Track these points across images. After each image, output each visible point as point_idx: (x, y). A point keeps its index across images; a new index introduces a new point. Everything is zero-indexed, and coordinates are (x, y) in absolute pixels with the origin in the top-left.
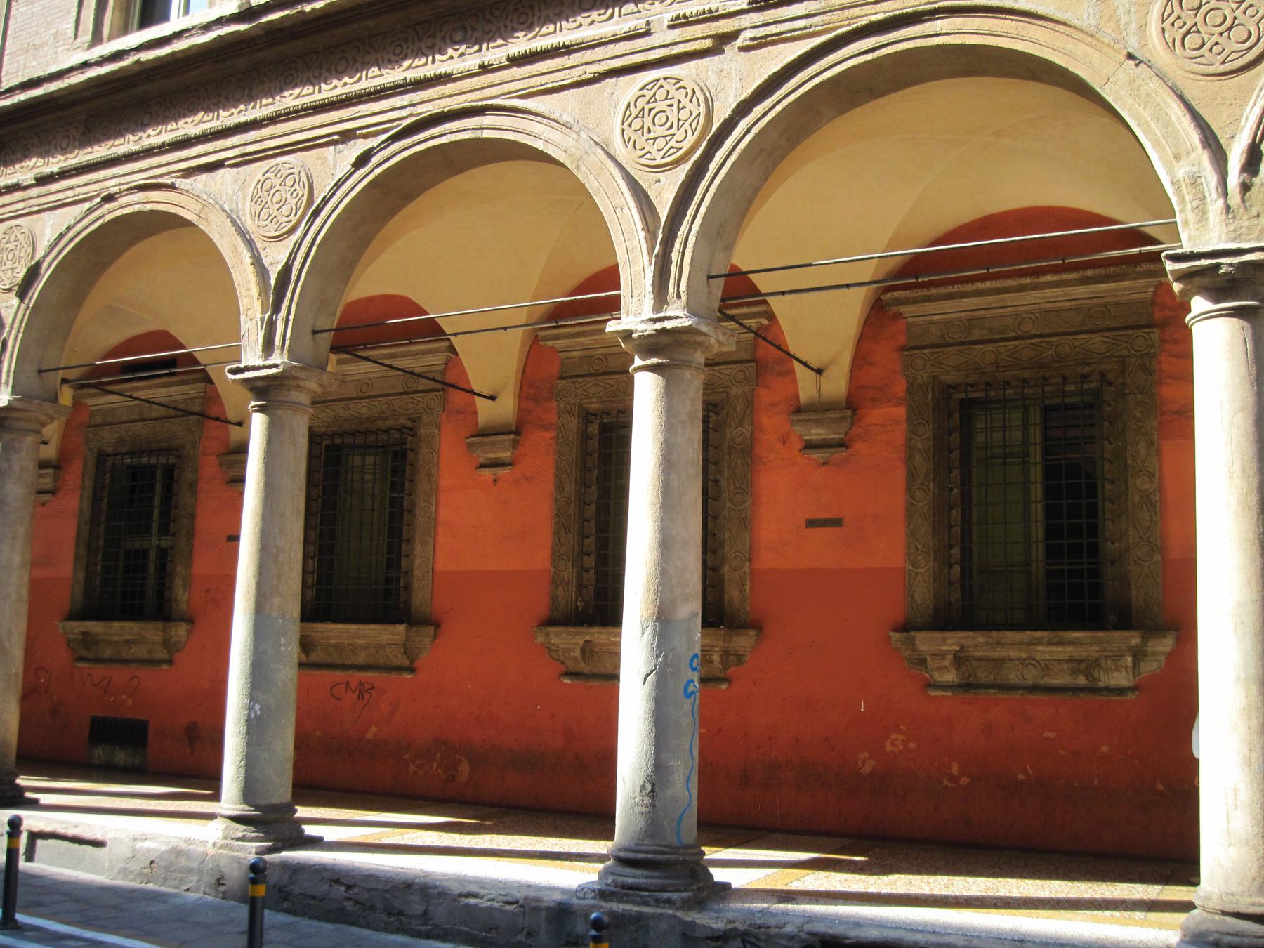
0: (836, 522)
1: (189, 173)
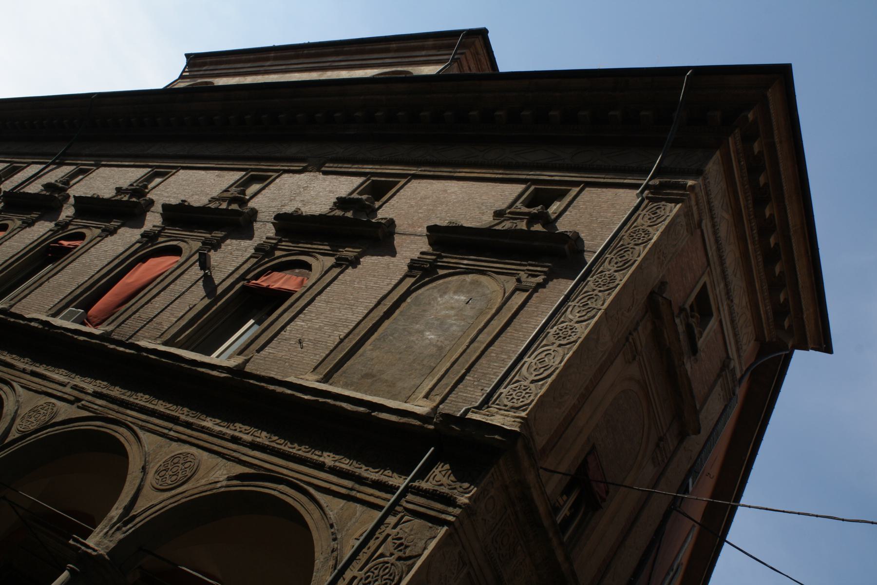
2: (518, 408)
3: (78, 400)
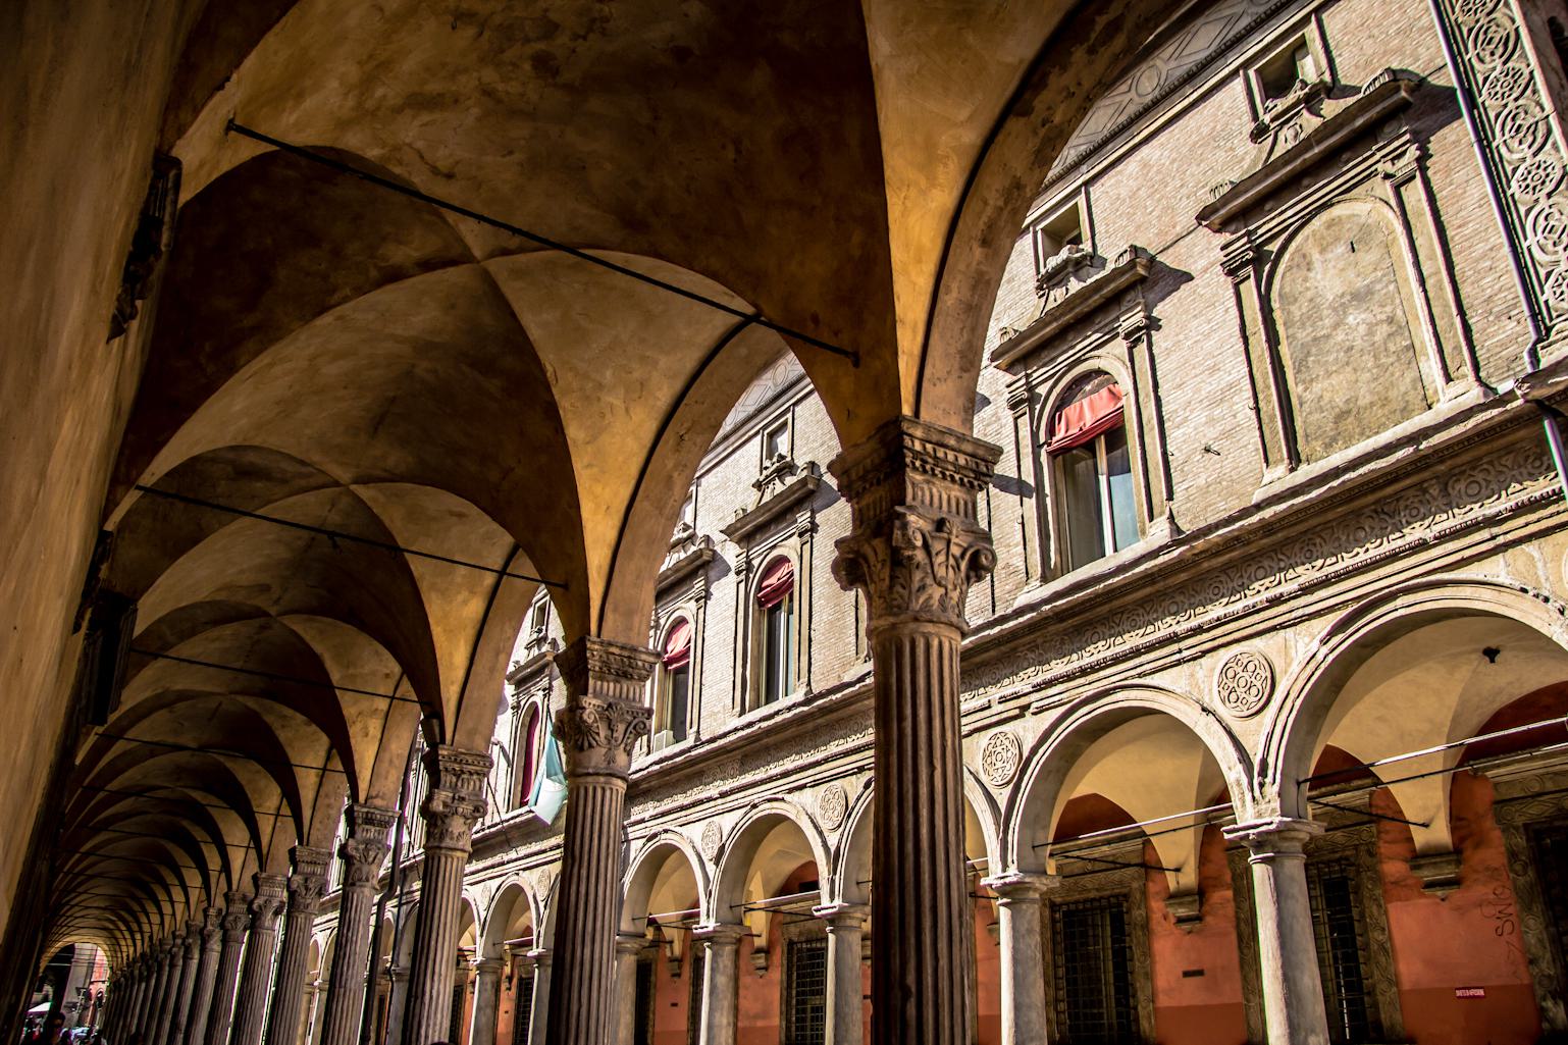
0: (1200, 973)
1: (790, 791)
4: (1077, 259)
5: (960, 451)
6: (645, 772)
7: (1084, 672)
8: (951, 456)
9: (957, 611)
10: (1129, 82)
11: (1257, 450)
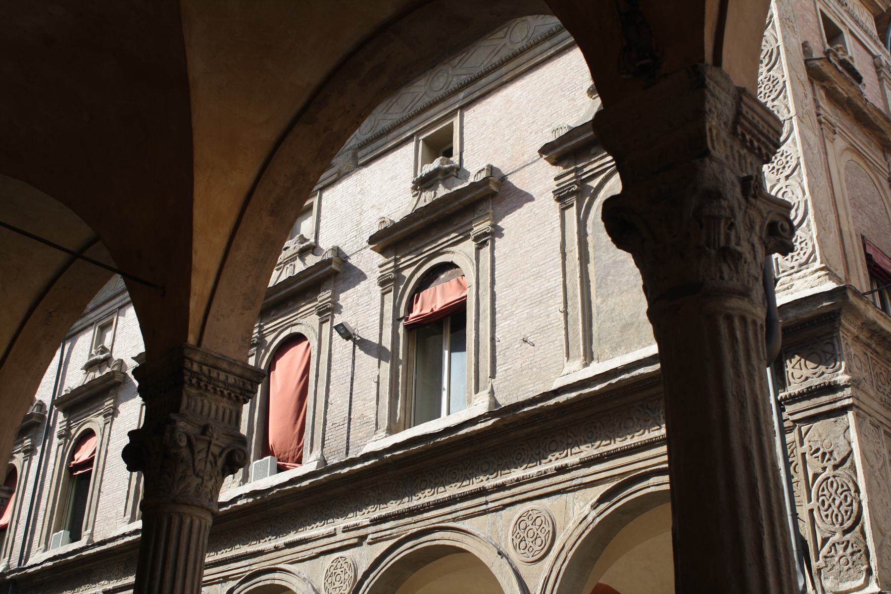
2: (806, 262)
3: (363, 538)
4: (446, 169)
5: (231, 373)
6: (39, 567)
7: (412, 512)
8: (222, 376)
9: (209, 496)
10: (506, 29)
11: (562, 345)
